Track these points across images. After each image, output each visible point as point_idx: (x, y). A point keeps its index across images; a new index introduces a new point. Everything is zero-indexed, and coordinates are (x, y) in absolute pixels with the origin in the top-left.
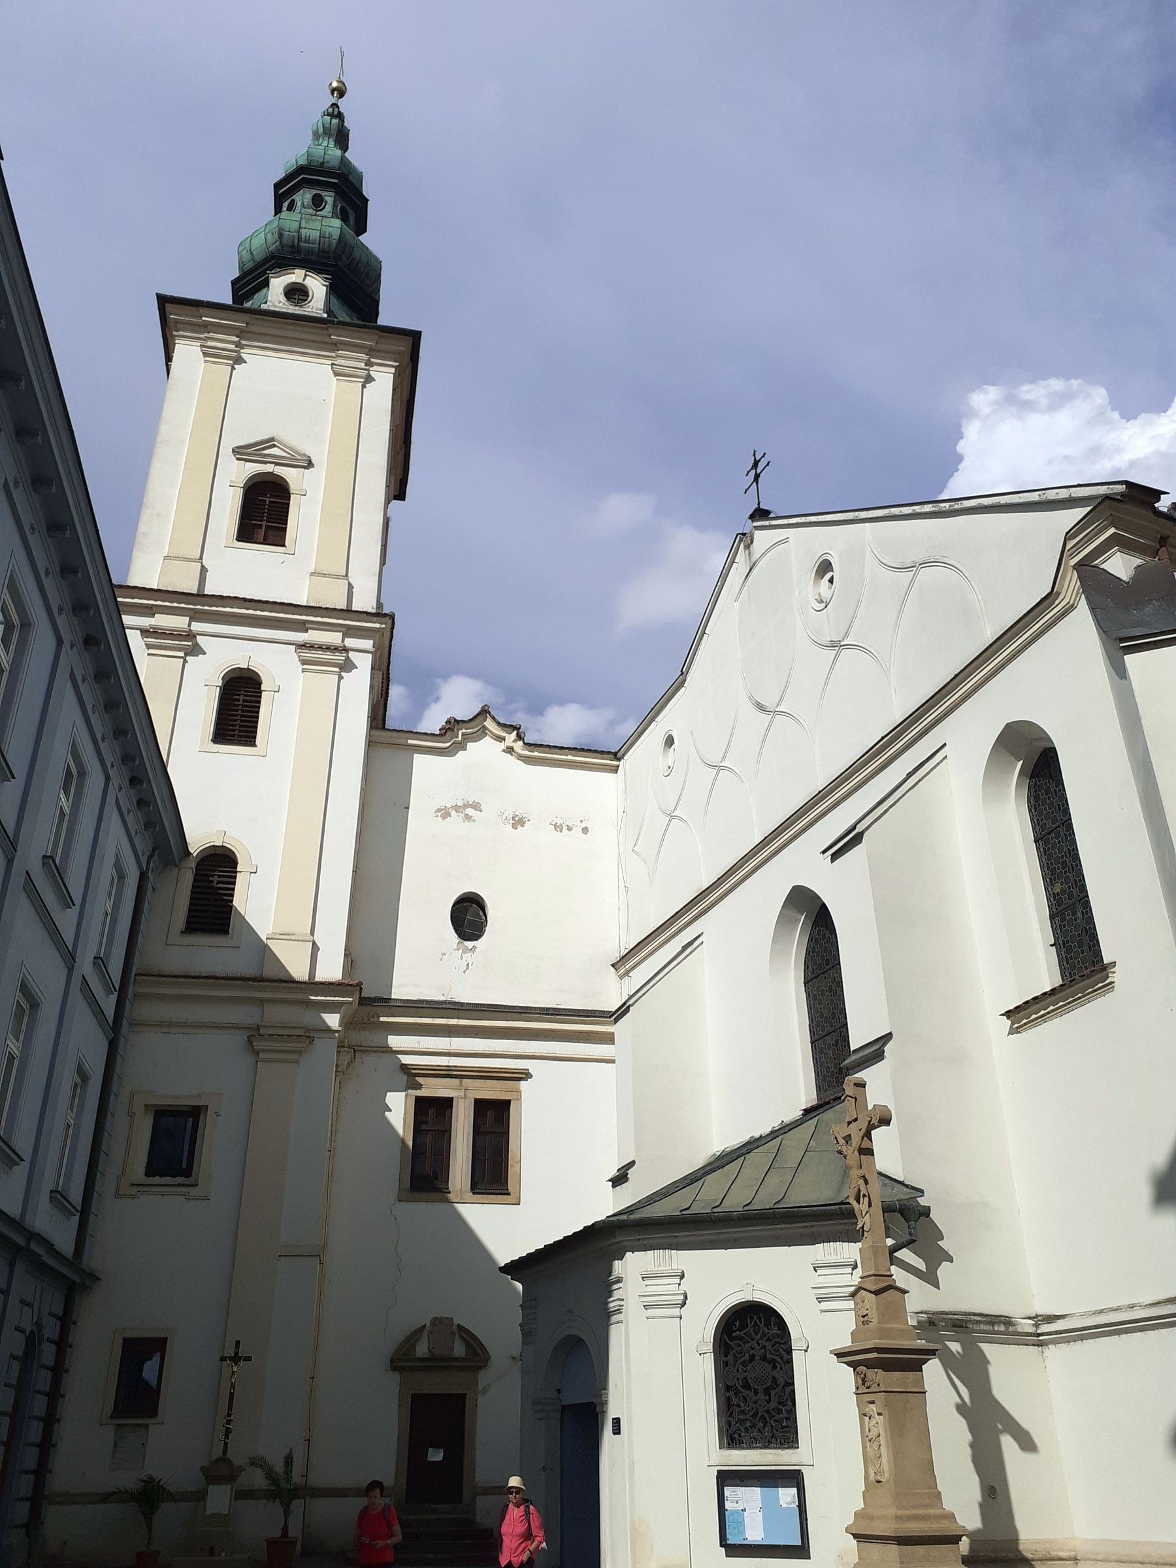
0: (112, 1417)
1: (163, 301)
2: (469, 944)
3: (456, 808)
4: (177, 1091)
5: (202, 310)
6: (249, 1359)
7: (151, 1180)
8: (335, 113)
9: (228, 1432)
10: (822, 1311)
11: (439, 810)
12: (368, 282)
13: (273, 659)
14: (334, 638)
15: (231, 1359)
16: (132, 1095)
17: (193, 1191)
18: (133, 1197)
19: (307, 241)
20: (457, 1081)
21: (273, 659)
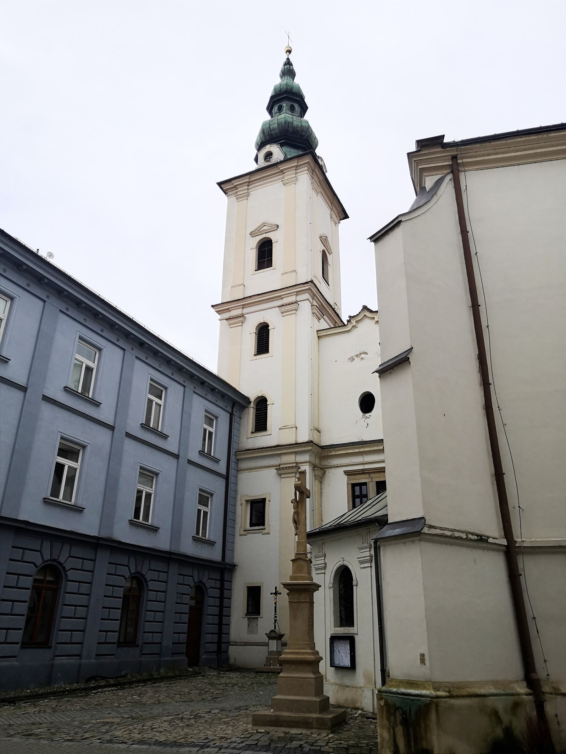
0: (246, 615)
1: (220, 184)
2: (367, 415)
3: (357, 356)
4: (256, 494)
5: (233, 182)
6: (280, 593)
7: (252, 528)
8: (288, 63)
9: (275, 621)
10: (361, 568)
11: (349, 359)
12: (303, 133)
13: (270, 315)
14: (292, 299)
15: (274, 594)
16: (241, 496)
17: (264, 531)
18: (245, 535)
19: (274, 130)
20: (367, 475)
21: (270, 315)
